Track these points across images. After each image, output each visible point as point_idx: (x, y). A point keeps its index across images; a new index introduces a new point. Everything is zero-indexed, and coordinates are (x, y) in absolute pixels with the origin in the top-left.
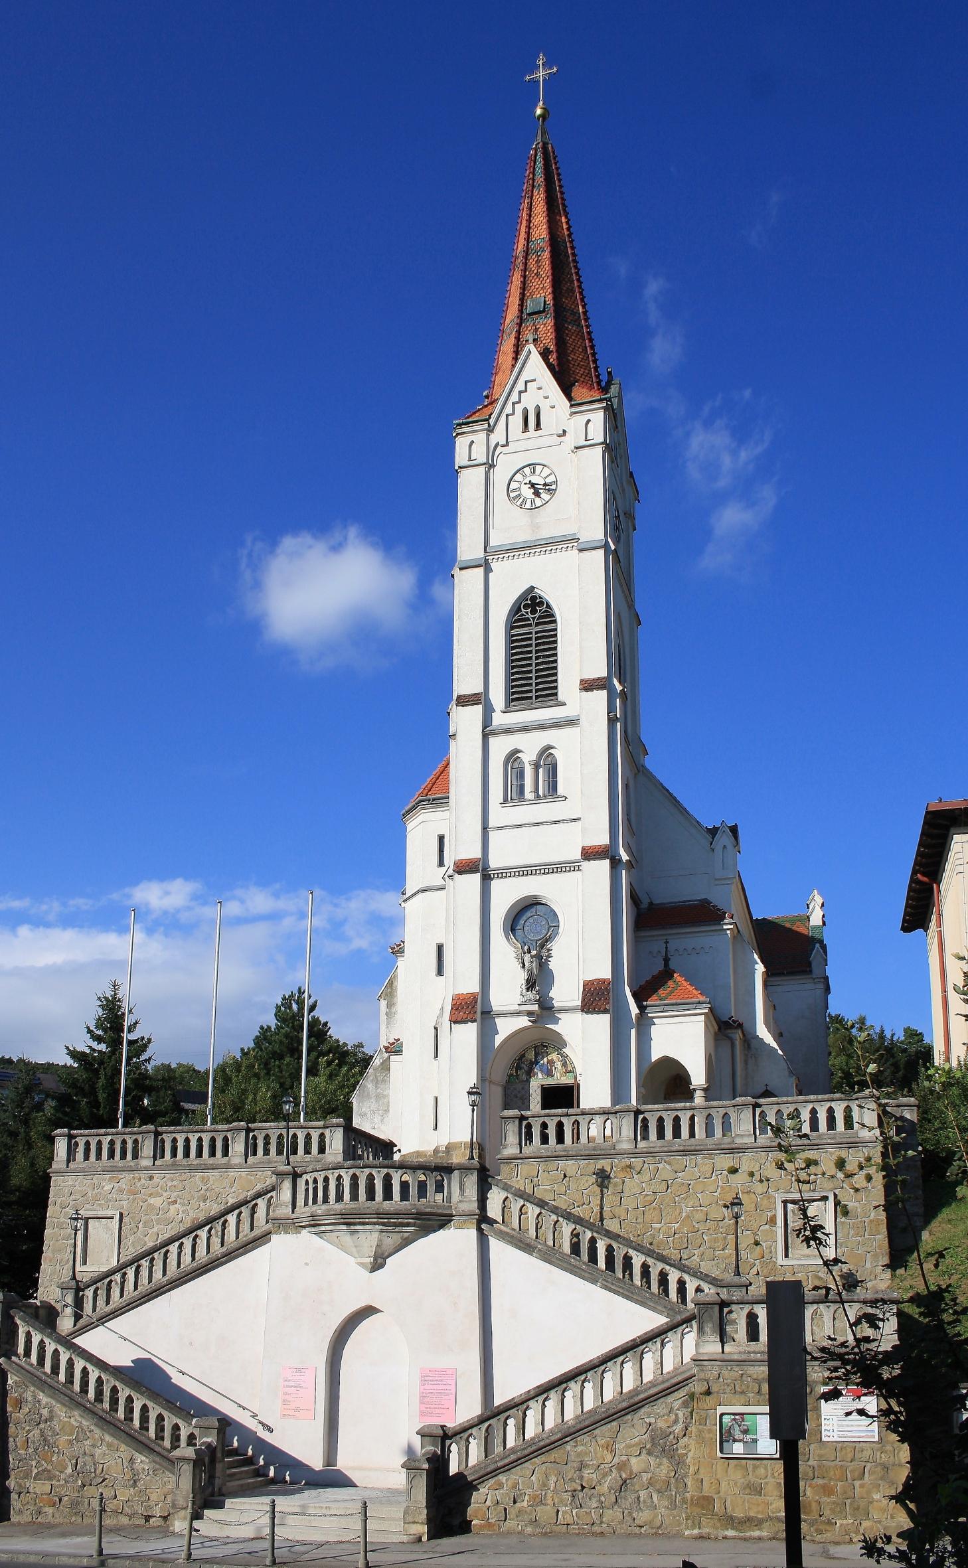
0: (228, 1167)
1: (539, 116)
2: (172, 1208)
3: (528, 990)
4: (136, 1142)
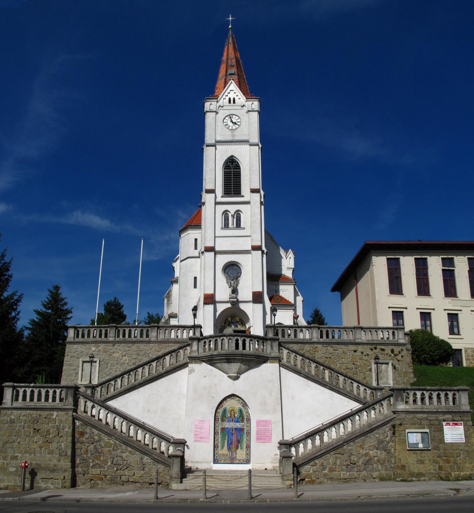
0: (150, 342)
2: (124, 358)
3: (232, 293)
4: (106, 331)
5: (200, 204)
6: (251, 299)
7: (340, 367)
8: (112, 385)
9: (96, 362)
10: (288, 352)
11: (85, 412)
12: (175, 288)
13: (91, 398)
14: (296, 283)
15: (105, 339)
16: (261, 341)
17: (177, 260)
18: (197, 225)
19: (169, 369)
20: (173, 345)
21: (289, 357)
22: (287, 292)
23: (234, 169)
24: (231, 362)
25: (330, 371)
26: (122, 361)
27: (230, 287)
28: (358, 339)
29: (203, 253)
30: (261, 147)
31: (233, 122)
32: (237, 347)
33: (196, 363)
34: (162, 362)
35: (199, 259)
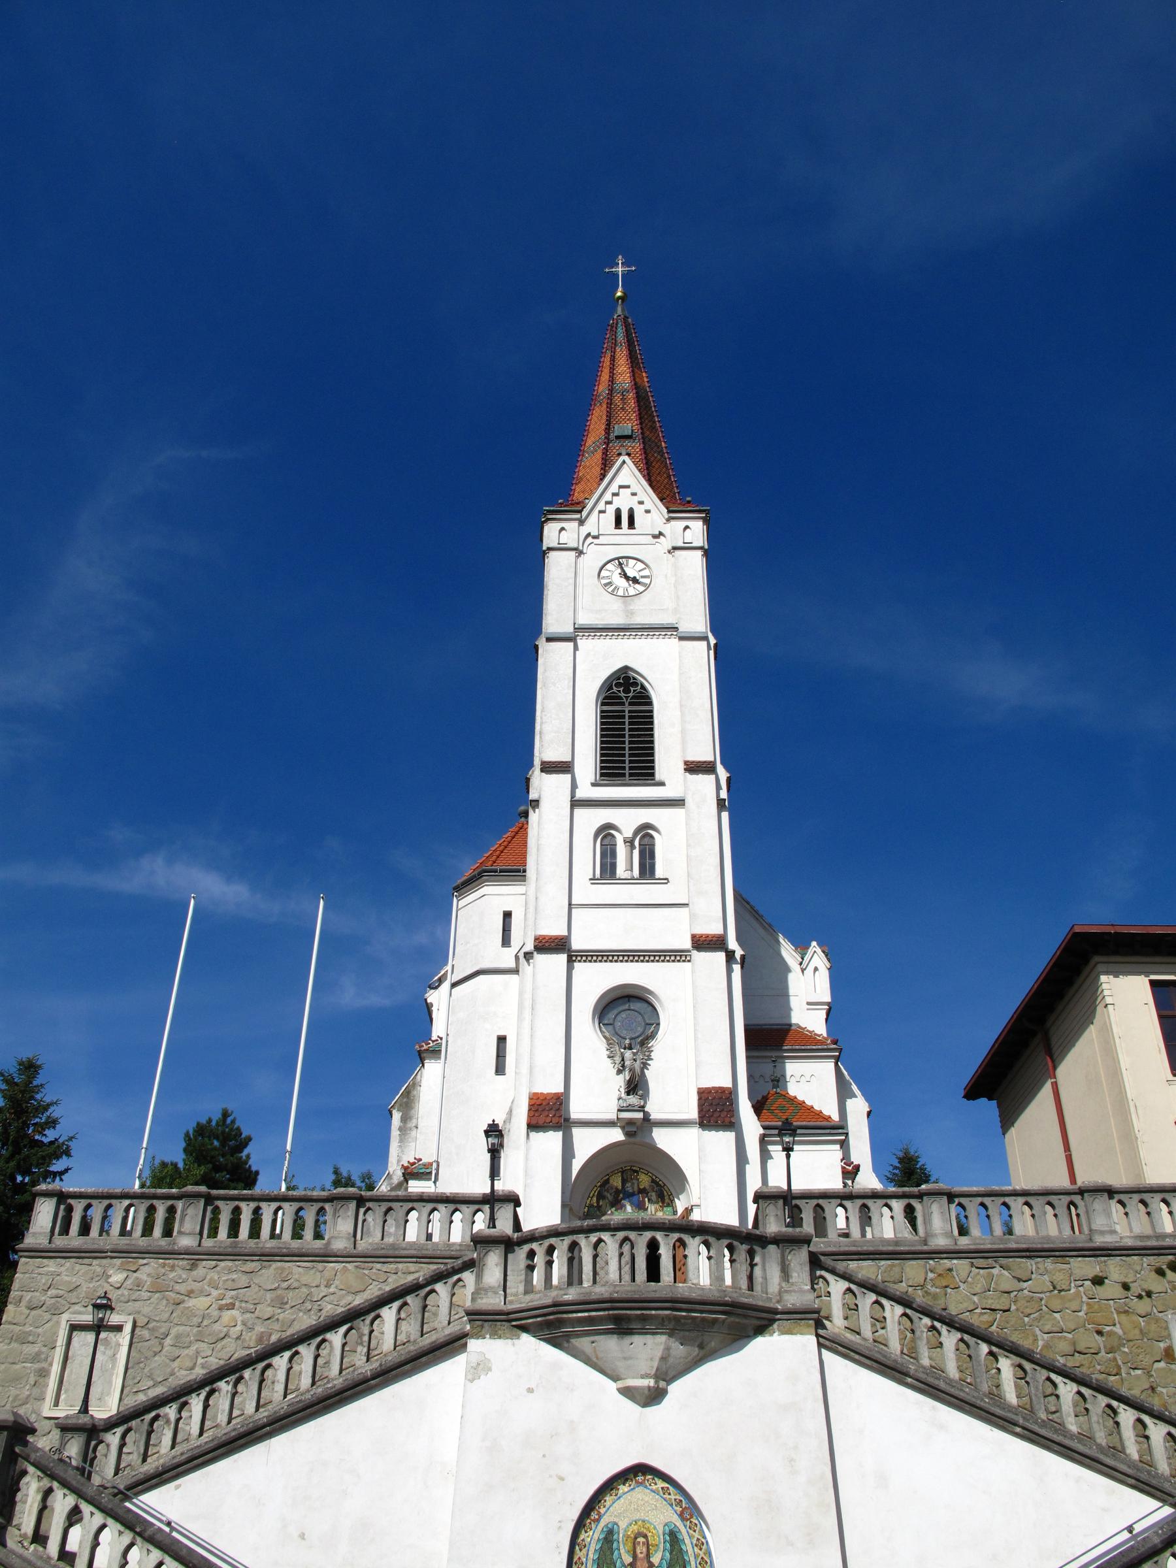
0: (326, 1256)
1: (619, 298)
2: (227, 1315)
3: (628, 1093)
4: (171, 1210)
5: (522, 808)
6: (693, 1113)
7: (1047, 1346)
8: (168, 1422)
9: (119, 1328)
10: (849, 1290)
11: (39, 1538)
12: (431, 1071)
13: (76, 1478)
14: (840, 1050)
15: (164, 1243)
16: (742, 1248)
17: (441, 981)
18: (516, 872)
19: (393, 1358)
20: (412, 1267)
21: (852, 1309)
22: (811, 1082)
23: (630, 704)
24: (629, 1332)
25: (1018, 1360)
26: (217, 1327)
27: (619, 1072)
28: (1102, 1233)
29: (528, 956)
30: (716, 645)
31: (627, 578)
32: (654, 1273)
33: (495, 1335)
34: (366, 1331)
35: (514, 978)
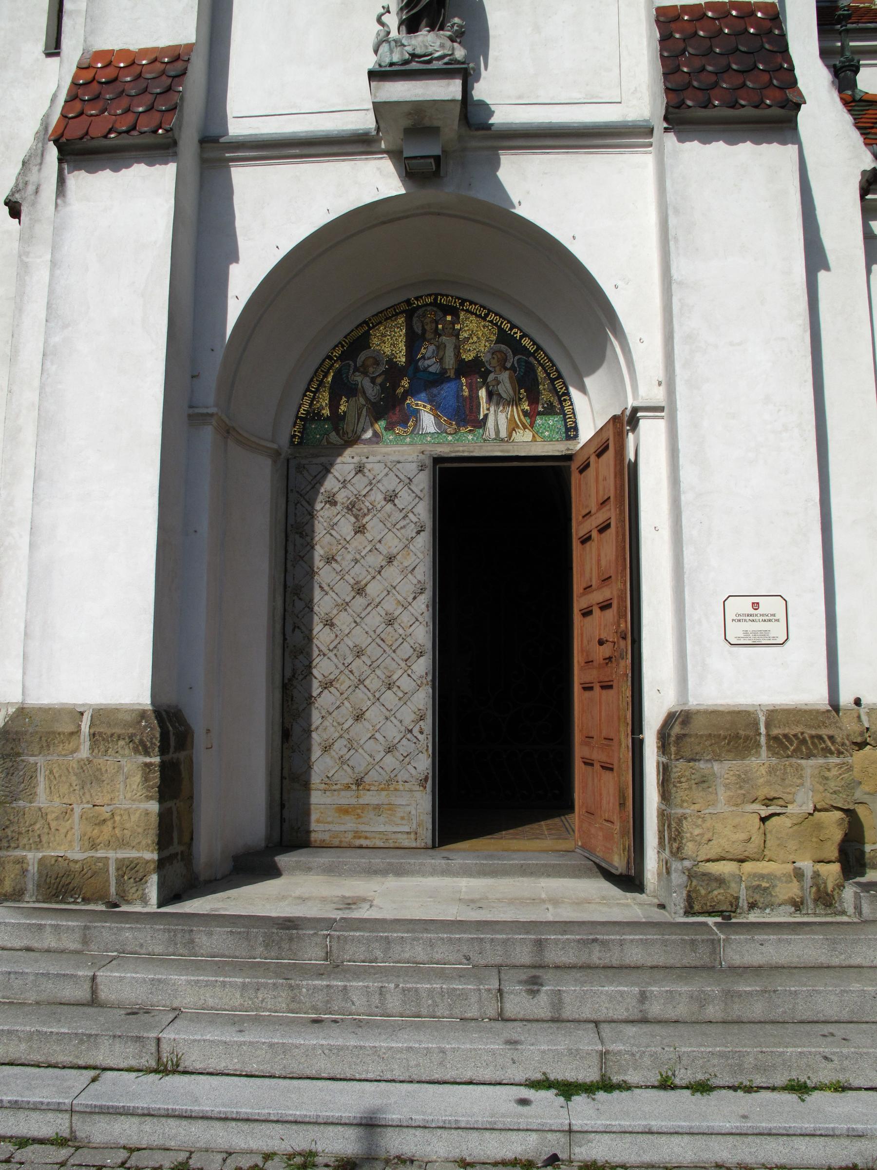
3: (411, 25)
